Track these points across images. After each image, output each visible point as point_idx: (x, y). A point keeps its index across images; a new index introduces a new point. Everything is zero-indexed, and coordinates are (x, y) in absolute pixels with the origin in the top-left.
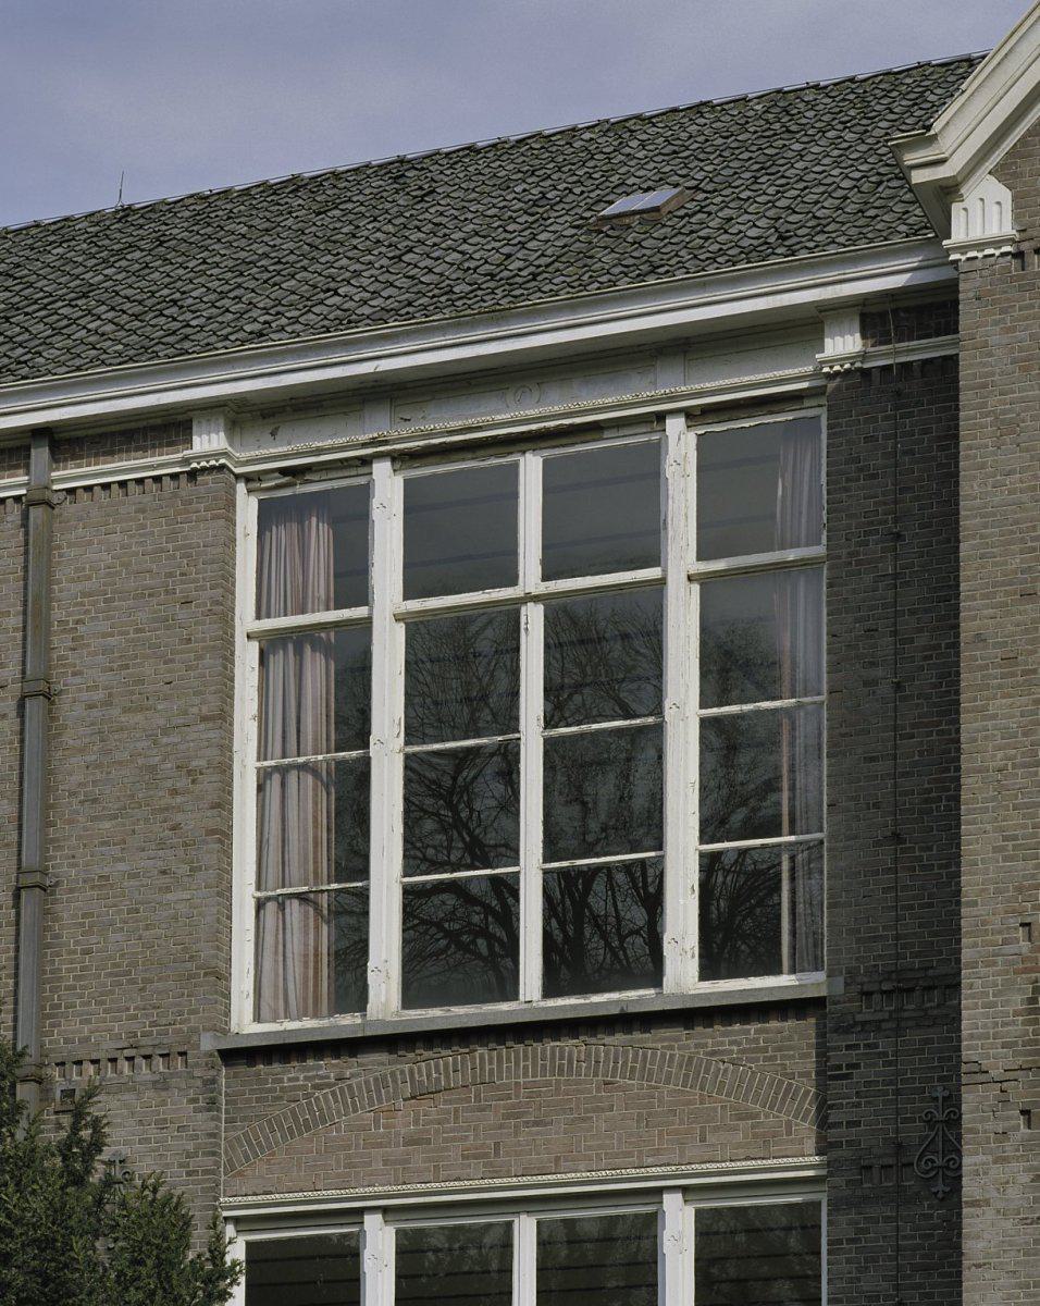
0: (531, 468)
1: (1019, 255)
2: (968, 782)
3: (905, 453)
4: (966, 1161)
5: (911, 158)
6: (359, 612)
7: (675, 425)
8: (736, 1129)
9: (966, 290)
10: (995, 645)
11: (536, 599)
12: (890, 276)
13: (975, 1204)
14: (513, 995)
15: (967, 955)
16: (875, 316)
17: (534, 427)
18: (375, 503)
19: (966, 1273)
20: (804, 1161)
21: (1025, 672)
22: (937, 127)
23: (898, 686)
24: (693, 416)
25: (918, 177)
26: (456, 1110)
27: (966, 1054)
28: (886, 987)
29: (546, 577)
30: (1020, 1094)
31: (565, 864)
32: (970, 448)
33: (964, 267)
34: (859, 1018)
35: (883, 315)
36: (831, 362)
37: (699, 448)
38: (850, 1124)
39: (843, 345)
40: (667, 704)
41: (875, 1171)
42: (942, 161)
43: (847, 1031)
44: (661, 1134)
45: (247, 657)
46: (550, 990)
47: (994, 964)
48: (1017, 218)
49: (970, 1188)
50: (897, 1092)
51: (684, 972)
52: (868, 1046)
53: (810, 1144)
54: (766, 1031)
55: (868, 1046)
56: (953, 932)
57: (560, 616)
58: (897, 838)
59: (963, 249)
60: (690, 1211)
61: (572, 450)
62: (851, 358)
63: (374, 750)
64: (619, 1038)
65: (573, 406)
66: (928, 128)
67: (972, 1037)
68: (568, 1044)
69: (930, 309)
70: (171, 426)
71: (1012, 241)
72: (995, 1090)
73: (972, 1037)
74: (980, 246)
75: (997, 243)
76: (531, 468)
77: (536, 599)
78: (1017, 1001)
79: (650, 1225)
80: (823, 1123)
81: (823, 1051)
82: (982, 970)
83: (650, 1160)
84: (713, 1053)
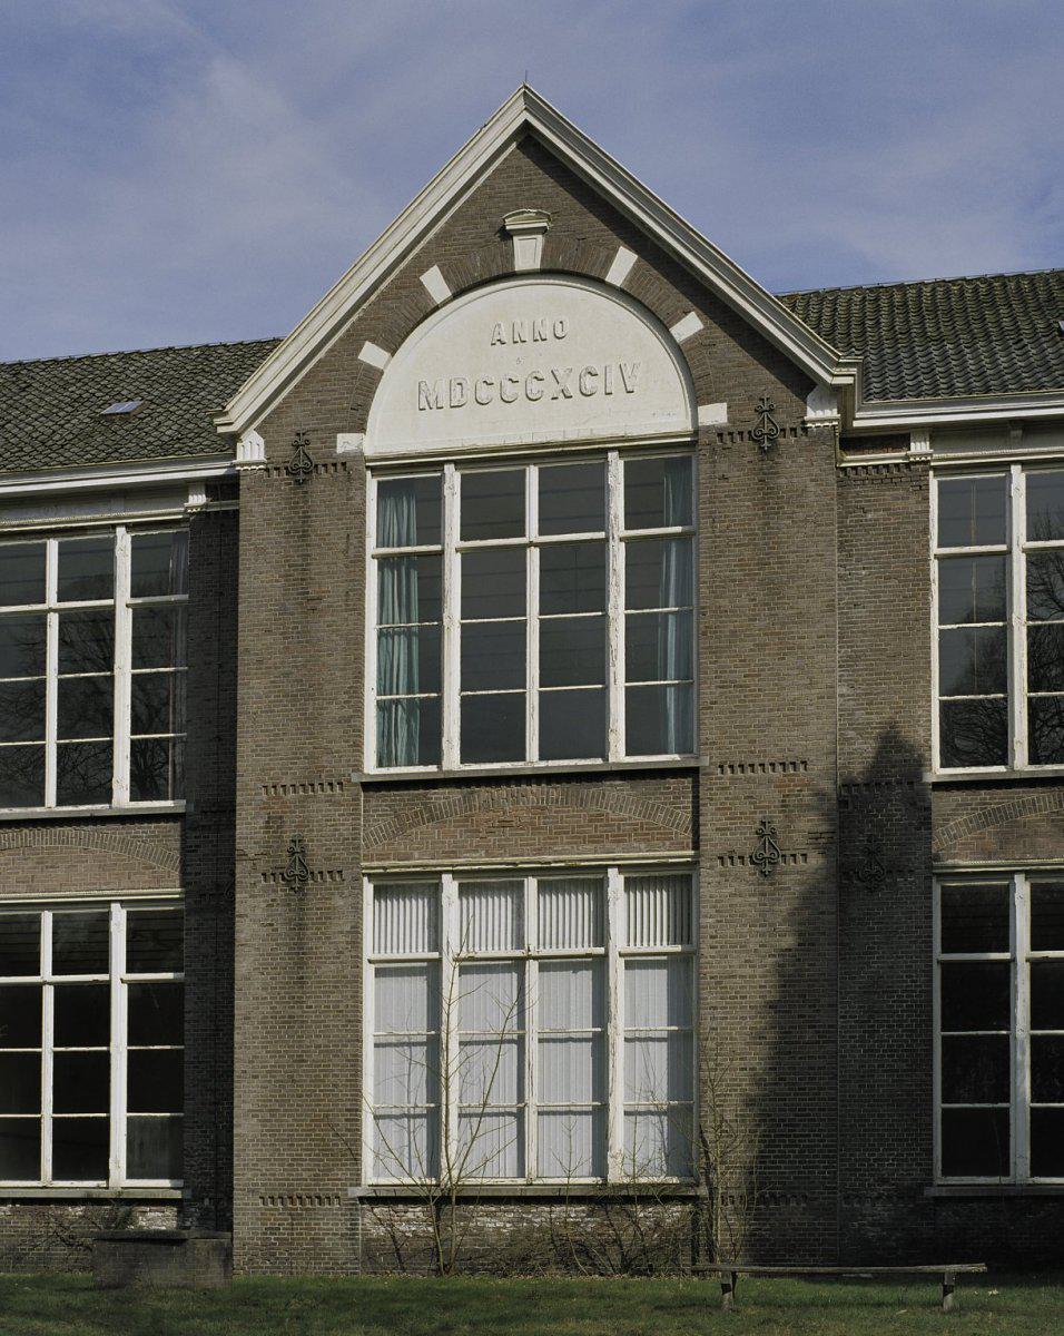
0: (53, 547)
1: (267, 470)
2: (240, 718)
3: (225, 554)
4: (238, 896)
5: (217, 421)
6: (109, 602)
7: (121, 531)
8: (144, 874)
9: (243, 483)
10: (254, 654)
11: (55, 611)
12: (217, 470)
13: (241, 916)
14: (42, 803)
15: (239, 799)
16: (212, 487)
17: (53, 526)
18: (117, 547)
19: (236, 949)
20: (173, 890)
21: (267, 668)
22: (228, 408)
23: (220, 666)
24: (129, 527)
25: (221, 430)
26: (596, 826)
27: (238, 846)
28: (213, 809)
29: (59, 601)
30: (262, 865)
31: (67, 741)
32: (243, 560)
33: (242, 474)
34: (202, 823)
35: (216, 487)
36: (192, 508)
37: (132, 542)
38: (196, 874)
39: (197, 500)
40: (116, 666)
41: (207, 896)
42: (231, 424)
43: (195, 829)
44: (110, 875)
45: (934, 566)
46: (60, 802)
47: (251, 804)
48: (266, 452)
49: (239, 909)
50: (217, 859)
51: (122, 797)
52: (205, 837)
53: (178, 883)
54: (159, 827)
55: (205, 837)
56: (233, 792)
57: (66, 619)
58: (219, 738)
59: (242, 465)
60: (124, 912)
61: (73, 539)
62: (202, 507)
63: (116, 671)
64: (91, 827)
65: (72, 518)
66: (224, 408)
67: (240, 838)
68: (67, 829)
69: (225, 488)
70: (897, 438)
71: (264, 463)
72: (250, 864)
73: (240, 838)
74: (250, 464)
75: (257, 464)
76: (53, 547)
77: (55, 611)
78: (261, 823)
79: (105, 919)
80: (183, 873)
81: (184, 838)
82: (245, 807)
83: (104, 887)
84: (134, 837)
